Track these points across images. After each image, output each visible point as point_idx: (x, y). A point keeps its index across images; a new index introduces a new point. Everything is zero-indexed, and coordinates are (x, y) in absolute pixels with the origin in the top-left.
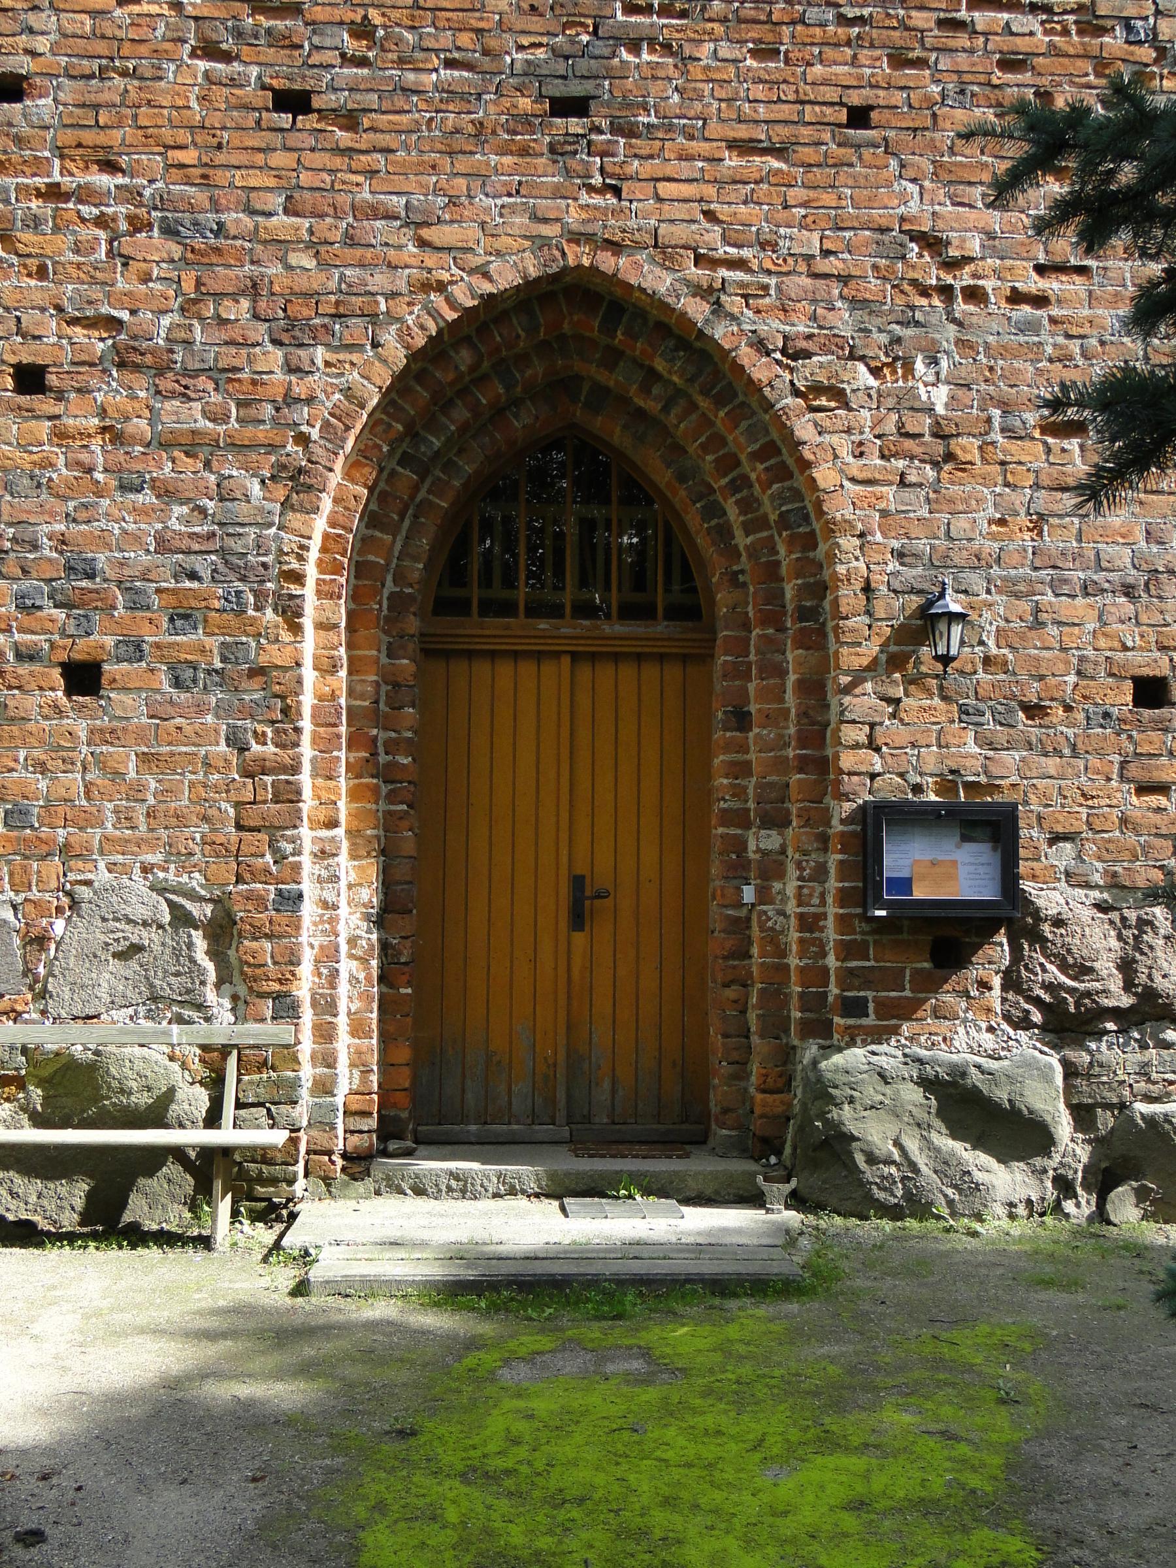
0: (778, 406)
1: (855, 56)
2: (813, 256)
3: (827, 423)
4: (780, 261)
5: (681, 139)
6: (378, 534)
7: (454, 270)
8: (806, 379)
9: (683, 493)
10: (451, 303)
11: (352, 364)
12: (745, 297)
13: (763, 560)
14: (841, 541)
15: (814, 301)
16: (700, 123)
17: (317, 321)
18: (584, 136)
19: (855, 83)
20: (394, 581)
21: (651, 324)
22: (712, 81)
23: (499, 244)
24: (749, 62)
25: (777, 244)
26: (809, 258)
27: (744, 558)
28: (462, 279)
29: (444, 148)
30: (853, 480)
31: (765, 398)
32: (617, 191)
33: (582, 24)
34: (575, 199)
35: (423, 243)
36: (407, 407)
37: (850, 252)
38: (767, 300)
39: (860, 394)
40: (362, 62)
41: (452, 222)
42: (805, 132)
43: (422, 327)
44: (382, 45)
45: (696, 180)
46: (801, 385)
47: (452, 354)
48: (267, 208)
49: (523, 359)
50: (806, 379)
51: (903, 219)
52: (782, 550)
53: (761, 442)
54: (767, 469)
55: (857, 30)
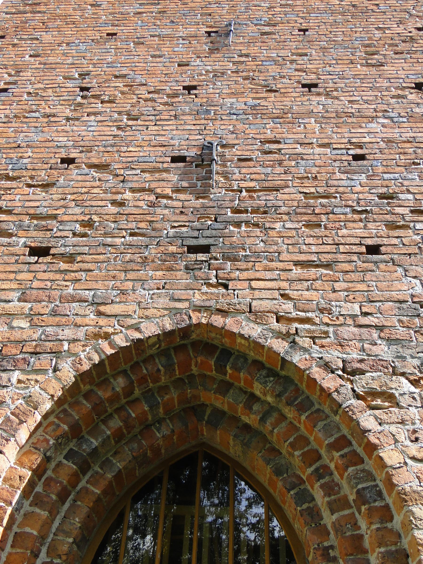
0: (344, 406)
1: (365, 225)
2: (357, 316)
3: (384, 417)
4: (335, 319)
5: (265, 261)
6: (38, 510)
7: (117, 327)
8: (363, 387)
9: (280, 484)
10: (112, 345)
11: (37, 381)
12: (313, 338)
13: (348, 534)
14: (414, 509)
15: (361, 340)
16: (277, 254)
17: (21, 356)
18: (206, 261)
19: (368, 236)
20: (48, 553)
21: (250, 361)
22: (283, 237)
23: (147, 313)
24: (303, 229)
25: (331, 310)
26: (354, 317)
27: (332, 536)
28: (121, 332)
29: (122, 269)
30: (413, 458)
31: (335, 399)
32: (226, 287)
33: (208, 217)
34: (199, 290)
35: (100, 314)
36: (74, 413)
37: (381, 313)
38: (328, 340)
39: (406, 397)
40: (84, 235)
41: (120, 302)
42: (341, 257)
43: (90, 359)
44: (96, 228)
45: (275, 280)
46: (360, 391)
47: (112, 380)
48: (7, 298)
49: (164, 389)
50: (363, 387)
51: (412, 296)
52: (363, 524)
53: (336, 436)
54: (342, 456)
55: (364, 216)
